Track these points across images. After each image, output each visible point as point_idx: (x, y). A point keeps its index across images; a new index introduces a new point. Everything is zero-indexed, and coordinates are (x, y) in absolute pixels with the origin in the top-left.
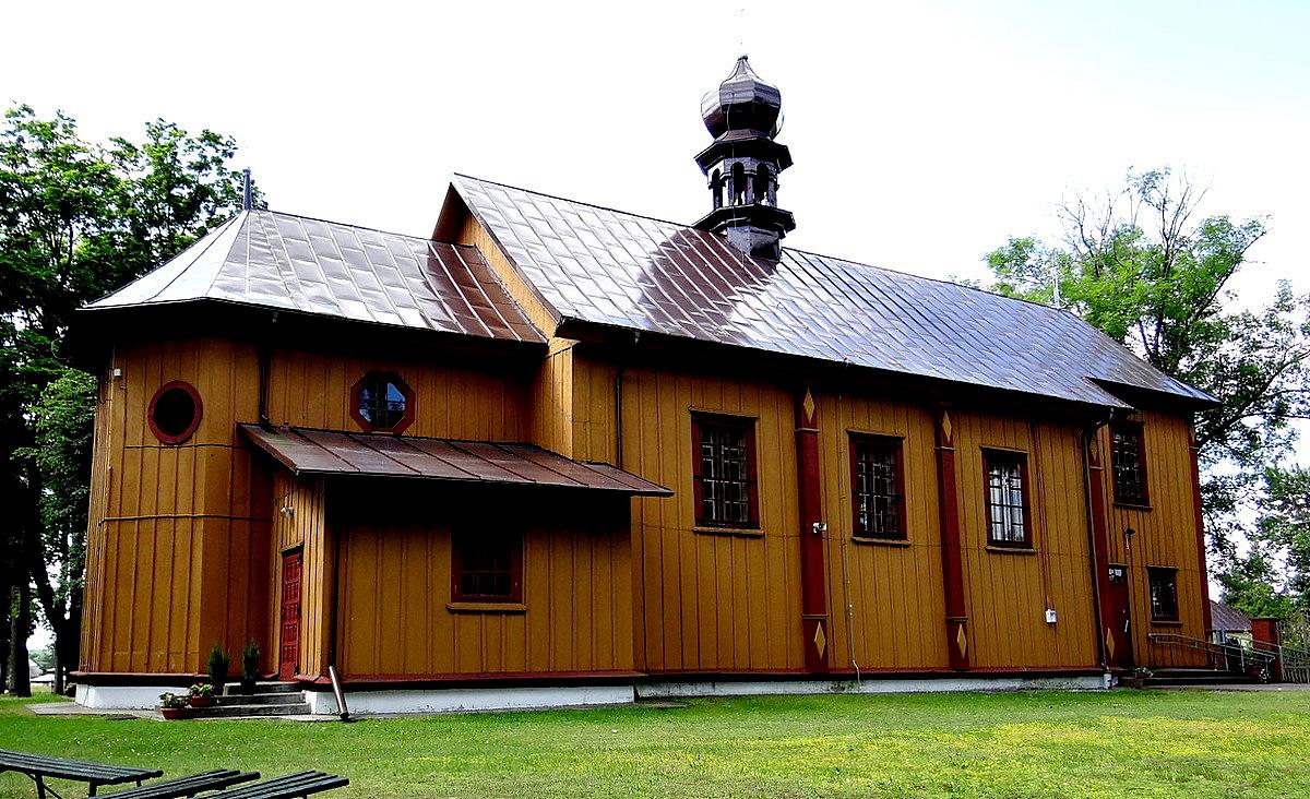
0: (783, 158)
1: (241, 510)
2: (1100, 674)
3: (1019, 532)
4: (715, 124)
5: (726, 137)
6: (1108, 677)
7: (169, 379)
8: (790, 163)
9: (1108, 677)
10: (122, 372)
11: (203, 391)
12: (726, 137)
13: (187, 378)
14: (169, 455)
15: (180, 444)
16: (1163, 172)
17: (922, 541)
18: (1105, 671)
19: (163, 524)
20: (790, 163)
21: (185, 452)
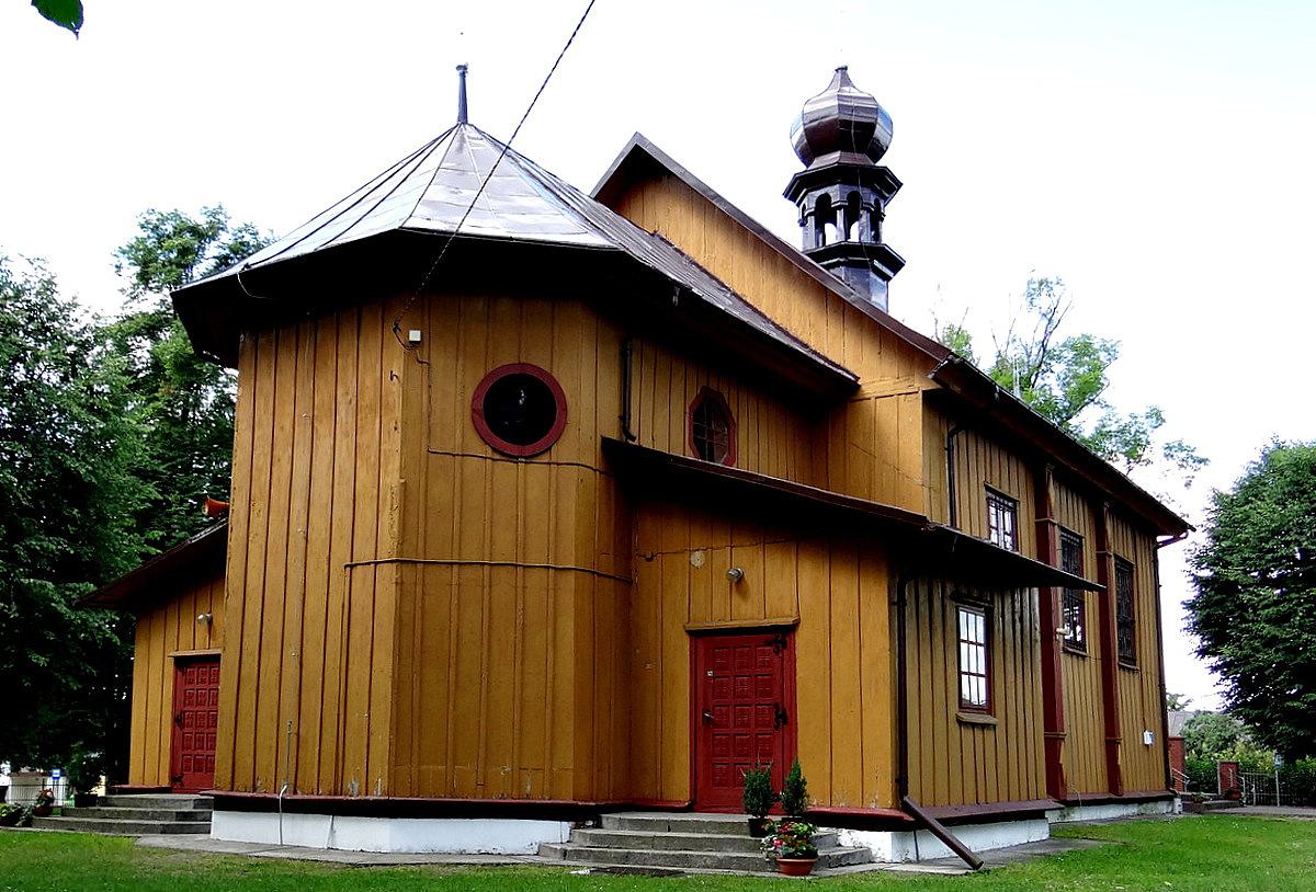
0: (887, 185)
1: (607, 564)
2: (1170, 799)
3: (1079, 638)
4: (809, 151)
5: (821, 162)
6: (1178, 801)
7: (507, 357)
8: (900, 185)
9: (1178, 801)
10: (57, 768)
11: (566, 385)
12: (821, 162)
13: (539, 360)
14: (506, 472)
15: (530, 458)
16: (1055, 282)
17: (1093, 656)
18: (1176, 795)
19: (536, 578)
20: (900, 185)
21: (536, 473)
